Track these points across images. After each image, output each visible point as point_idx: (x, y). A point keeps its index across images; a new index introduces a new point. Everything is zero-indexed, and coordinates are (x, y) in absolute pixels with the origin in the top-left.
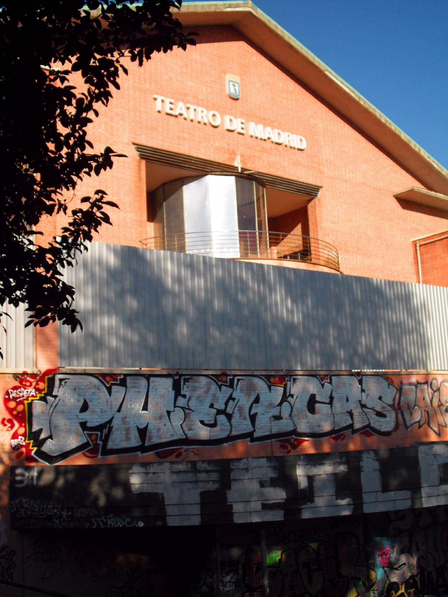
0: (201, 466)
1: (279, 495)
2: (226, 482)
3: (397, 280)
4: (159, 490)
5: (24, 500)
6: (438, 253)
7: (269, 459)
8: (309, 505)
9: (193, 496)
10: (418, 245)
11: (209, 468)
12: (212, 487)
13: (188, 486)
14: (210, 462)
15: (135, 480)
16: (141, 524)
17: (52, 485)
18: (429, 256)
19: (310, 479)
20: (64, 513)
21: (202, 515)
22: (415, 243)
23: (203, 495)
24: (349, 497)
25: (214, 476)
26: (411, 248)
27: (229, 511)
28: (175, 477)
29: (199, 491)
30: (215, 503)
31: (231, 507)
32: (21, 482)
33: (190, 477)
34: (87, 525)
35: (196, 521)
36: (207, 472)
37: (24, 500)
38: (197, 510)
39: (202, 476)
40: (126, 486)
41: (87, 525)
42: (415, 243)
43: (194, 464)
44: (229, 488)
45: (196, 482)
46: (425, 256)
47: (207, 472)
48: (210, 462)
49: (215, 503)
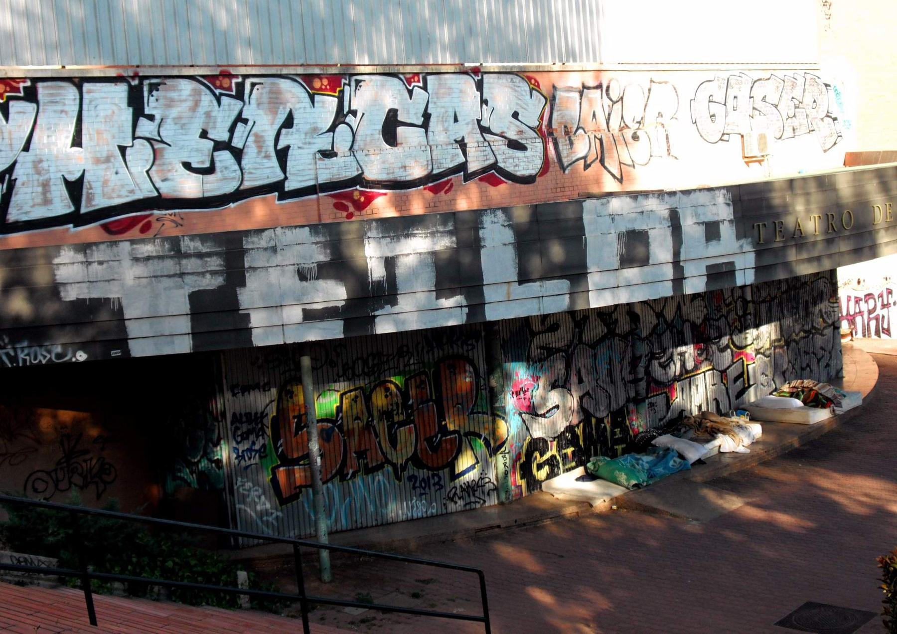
0: (188, 245)
1: (335, 293)
2: (235, 274)
7: (314, 229)
12: (211, 283)
14: (204, 238)
23: (195, 298)
24: (376, 335)
30: (217, 312)
33: (170, 266)
35: (184, 346)
36: (200, 255)
38: (185, 325)
39: (191, 264)
43: (175, 242)
48: (204, 238)
49: (217, 312)
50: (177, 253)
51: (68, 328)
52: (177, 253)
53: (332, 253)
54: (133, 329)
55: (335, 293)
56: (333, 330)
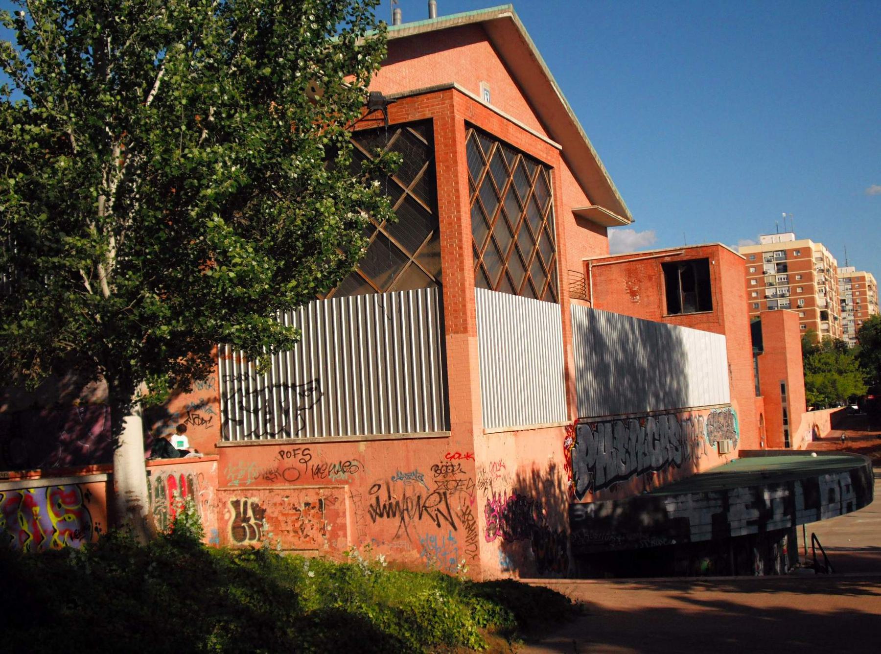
0: (712, 495)
1: (755, 514)
2: (726, 507)
3: (745, 307)
4: (685, 515)
5: (584, 530)
6: (614, 277)
7: (750, 488)
8: (771, 521)
9: (708, 519)
10: (590, 266)
11: (716, 497)
12: (719, 510)
13: (705, 511)
14: (716, 492)
15: (671, 508)
16: (674, 542)
17: (609, 518)
18: (603, 278)
19: (772, 501)
20: (619, 539)
21: (713, 532)
22: (587, 264)
23: (713, 516)
24: (698, 475)
25: (719, 503)
26: (582, 269)
27: (728, 529)
28: (695, 505)
29: (710, 514)
30: (720, 522)
31: (729, 525)
32: (580, 516)
33: (705, 503)
34: (636, 546)
35: (708, 537)
36: (715, 499)
37: (584, 530)
38: (709, 528)
39: (712, 503)
40: (665, 512)
41: (636, 546)
42: (587, 264)
43: (706, 494)
44: (729, 511)
45: (709, 507)
46: (598, 278)
47: (715, 499)
48: (716, 492)
49: (720, 522)
50: (707, 499)
51: (789, 440)
52: (707, 499)
53: (171, 415)
54: (693, 530)
55: (755, 514)
56: (754, 530)
